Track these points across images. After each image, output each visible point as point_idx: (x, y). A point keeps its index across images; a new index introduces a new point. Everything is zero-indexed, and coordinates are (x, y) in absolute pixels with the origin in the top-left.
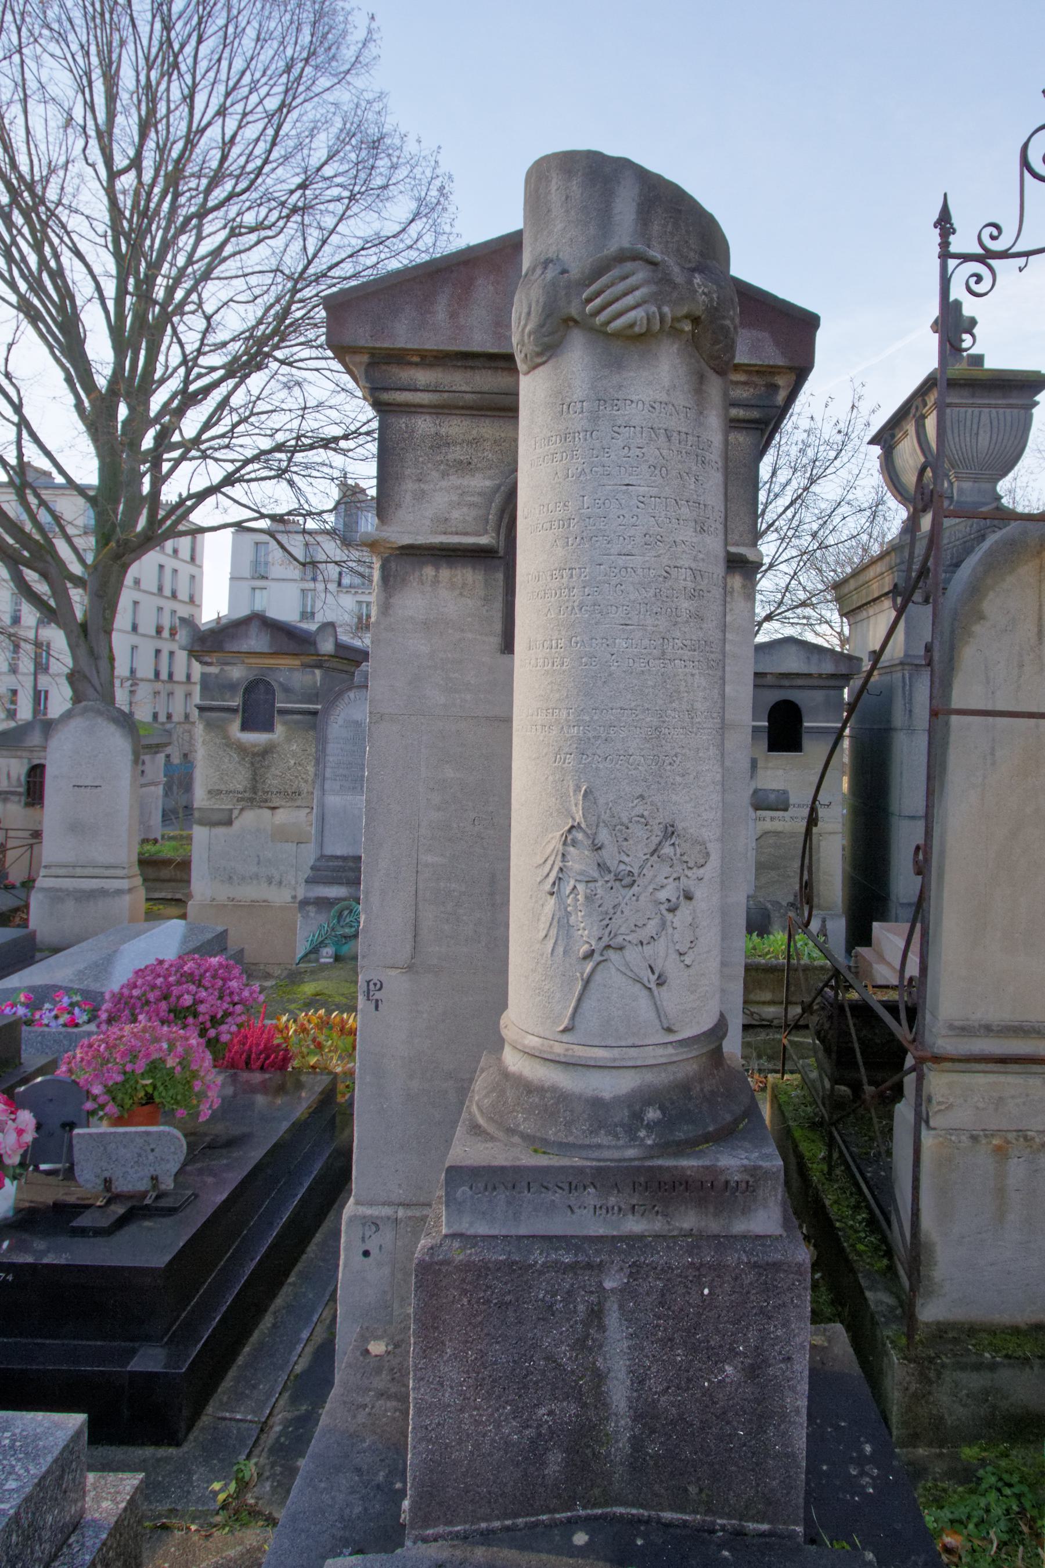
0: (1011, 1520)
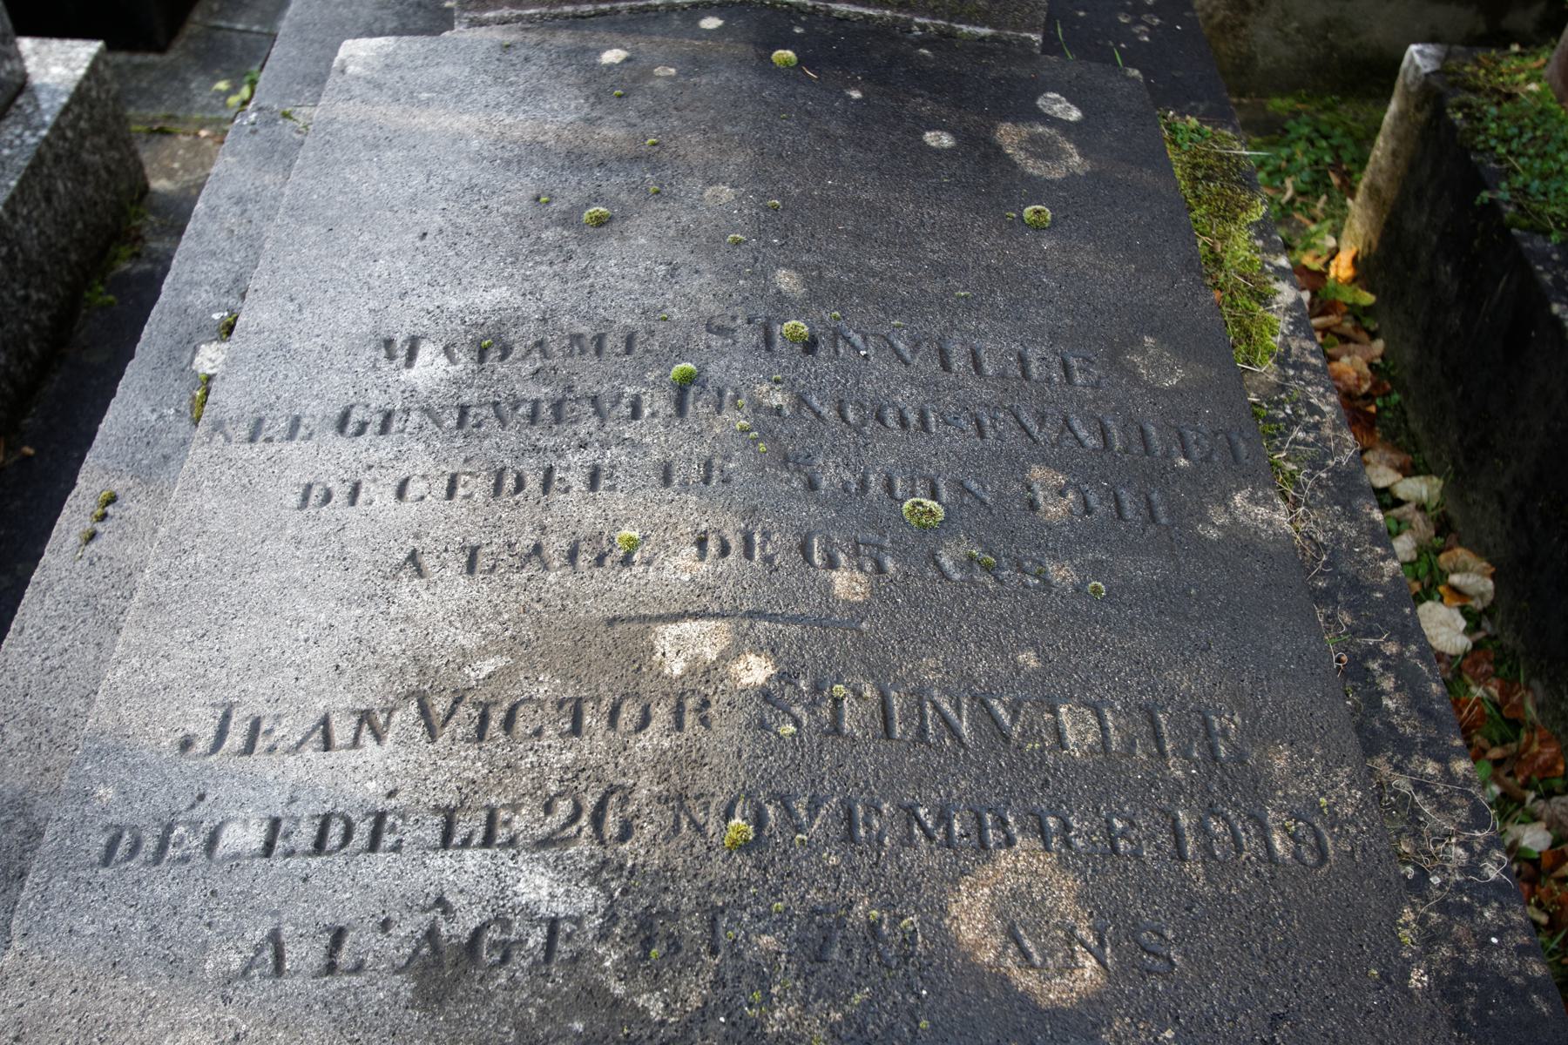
0: (1318, 172)
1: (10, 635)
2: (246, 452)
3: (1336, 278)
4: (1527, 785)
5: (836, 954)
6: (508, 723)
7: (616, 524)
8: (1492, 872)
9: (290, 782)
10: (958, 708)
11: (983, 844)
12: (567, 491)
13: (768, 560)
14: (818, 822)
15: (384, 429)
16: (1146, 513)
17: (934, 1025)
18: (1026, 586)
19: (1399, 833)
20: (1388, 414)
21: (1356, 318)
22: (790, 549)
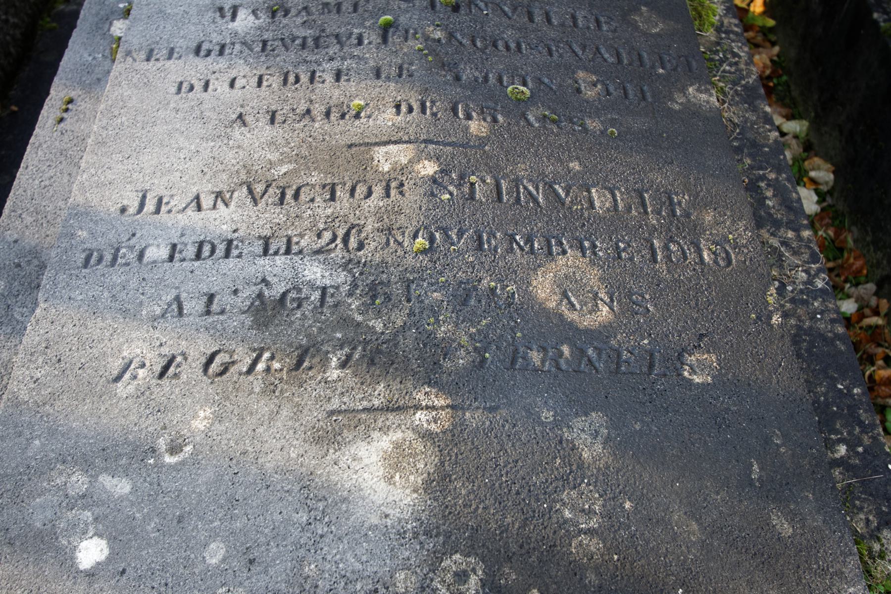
1: (21, 170)
2: (145, 66)
3: (754, 12)
4: (846, 281)
5: (473, 302)
6: (296, 196)
7: (351, 98)
8: (820, 284)
9: (180, 226)
10: (537, 189)
11: (550, 253)
12: (323, 82)
13: (434, 115)
14: (463, 241)
15: (221, 53)
16: (640, 95)
17: (524, 336)
18: (574, 130)
19: (771, 266)
20: (780, 88)
21: (765, 35)
22: (446, 110)
